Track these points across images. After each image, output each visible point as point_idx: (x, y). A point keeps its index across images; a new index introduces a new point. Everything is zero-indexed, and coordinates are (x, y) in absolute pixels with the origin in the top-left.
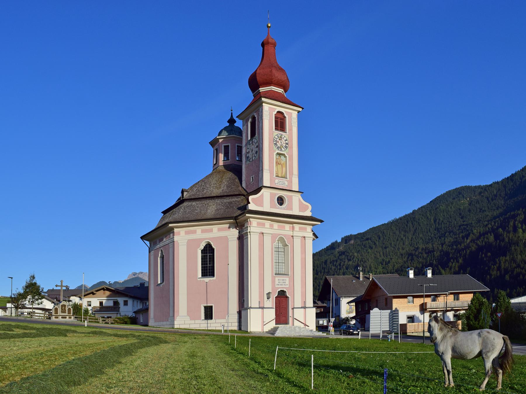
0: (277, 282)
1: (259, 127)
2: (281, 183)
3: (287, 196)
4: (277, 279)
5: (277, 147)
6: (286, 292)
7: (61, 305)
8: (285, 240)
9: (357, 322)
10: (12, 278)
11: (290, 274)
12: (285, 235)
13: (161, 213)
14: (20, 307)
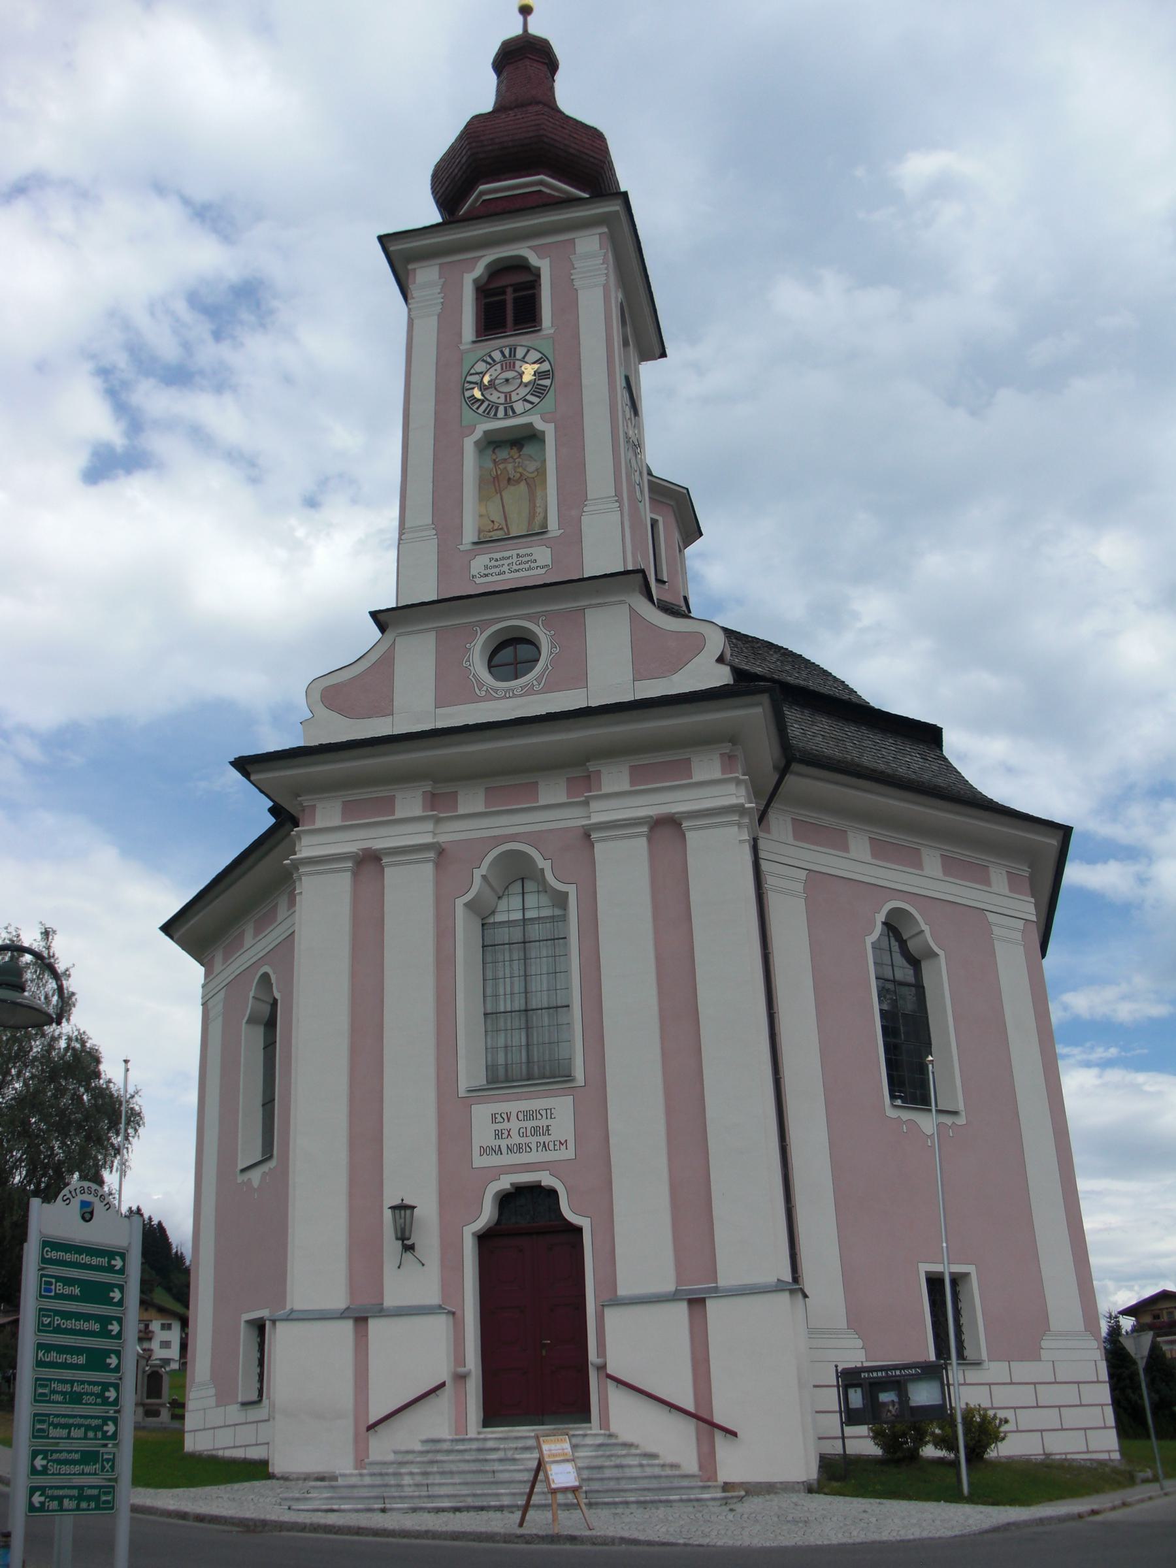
0: (482, 1132)
2: (505, 568)
3: (469, 694)
4: (481, 1113)
5: (535, 400)
6: (552, 1193)
8: (541, 863)
9: (701, 1423)
10: (268, 1444)
12: (534, 839)
13: (232, 763)
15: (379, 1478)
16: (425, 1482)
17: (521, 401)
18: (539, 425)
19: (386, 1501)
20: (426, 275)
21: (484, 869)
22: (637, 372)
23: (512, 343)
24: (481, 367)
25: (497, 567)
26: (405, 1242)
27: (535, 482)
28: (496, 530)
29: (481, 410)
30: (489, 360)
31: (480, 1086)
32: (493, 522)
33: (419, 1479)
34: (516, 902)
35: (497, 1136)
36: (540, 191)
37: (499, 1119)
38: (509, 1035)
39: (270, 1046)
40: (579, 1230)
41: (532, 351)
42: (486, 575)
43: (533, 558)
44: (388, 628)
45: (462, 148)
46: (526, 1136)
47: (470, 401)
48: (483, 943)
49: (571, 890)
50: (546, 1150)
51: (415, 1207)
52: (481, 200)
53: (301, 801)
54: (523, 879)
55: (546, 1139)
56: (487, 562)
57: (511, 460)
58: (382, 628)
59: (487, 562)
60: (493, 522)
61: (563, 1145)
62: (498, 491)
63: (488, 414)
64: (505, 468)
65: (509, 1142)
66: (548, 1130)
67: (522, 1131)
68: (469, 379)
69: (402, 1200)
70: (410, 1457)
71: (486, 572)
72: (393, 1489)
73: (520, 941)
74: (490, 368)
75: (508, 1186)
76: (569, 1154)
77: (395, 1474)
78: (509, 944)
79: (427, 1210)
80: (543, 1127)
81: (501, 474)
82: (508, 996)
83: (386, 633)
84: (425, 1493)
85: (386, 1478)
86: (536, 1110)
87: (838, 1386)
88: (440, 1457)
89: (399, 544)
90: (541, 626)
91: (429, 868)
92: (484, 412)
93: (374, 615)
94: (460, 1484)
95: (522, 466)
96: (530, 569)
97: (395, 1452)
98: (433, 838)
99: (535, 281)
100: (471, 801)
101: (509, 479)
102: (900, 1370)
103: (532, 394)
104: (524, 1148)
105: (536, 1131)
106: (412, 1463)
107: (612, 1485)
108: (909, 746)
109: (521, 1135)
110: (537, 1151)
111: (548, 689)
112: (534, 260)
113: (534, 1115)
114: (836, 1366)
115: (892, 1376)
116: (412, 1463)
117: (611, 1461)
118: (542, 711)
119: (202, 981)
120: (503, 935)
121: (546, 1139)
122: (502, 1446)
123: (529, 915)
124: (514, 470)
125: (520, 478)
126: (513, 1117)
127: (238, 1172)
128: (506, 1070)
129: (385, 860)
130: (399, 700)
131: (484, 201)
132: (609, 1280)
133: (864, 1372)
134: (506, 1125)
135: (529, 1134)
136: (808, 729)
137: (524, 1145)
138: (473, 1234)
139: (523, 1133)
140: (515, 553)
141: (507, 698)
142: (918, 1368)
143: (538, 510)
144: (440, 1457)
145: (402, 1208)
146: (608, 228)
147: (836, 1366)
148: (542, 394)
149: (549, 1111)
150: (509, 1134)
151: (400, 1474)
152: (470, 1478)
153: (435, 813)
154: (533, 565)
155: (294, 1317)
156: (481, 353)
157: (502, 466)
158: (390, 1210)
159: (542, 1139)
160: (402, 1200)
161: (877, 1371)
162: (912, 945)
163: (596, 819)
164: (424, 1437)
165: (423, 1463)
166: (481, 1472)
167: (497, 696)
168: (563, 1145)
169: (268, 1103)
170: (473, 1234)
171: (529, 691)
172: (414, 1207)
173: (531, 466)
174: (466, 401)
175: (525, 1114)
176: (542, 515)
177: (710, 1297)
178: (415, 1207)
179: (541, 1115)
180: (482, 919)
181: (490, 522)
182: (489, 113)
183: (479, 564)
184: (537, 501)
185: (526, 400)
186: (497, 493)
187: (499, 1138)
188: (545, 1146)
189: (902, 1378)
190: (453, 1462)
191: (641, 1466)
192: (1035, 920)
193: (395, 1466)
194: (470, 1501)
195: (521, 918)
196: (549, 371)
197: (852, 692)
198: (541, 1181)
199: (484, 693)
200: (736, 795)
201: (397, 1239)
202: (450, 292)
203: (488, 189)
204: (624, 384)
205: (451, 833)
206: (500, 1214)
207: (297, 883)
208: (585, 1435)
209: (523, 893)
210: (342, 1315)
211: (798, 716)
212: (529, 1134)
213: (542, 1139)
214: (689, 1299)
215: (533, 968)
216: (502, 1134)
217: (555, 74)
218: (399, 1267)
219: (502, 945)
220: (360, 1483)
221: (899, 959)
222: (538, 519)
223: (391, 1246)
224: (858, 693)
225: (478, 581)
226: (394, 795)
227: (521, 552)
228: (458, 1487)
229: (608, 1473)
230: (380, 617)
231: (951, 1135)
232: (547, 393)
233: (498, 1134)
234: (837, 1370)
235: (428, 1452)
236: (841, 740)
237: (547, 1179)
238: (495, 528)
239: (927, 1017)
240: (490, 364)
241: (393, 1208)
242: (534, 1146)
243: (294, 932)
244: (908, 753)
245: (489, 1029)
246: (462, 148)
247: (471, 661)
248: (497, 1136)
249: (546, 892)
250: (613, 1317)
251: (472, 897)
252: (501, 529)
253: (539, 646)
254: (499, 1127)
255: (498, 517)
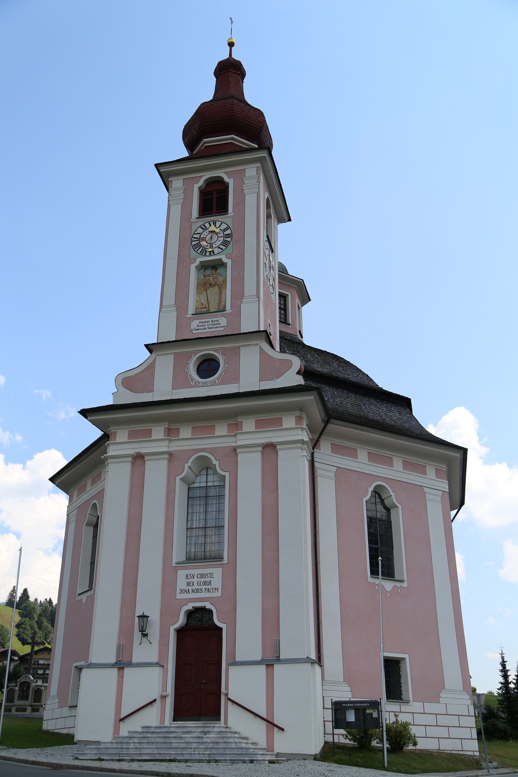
0: (181, 583)
1: (274, 235)
2: (206, 327)
3: (187, 384)
4: (181, 574)
5: (223, 248)
6: (210, 611)
7: (20, 683)
8: (215, 462)
11: (405, 578)
12: (212, 451)
14: (414, 738)
15: (120, 744)
16: (139, 747)
17: (217, 248)
18: (225, 260)
19: (121, 756)
20: (177, 183)
21: (189, 464)
22: (276, 229)
23: (214, 220)
24: (200, 230)
25: (202, 326)
26: (143, 633)
27: (222, 286)
28: (204, 308)
29: (199, 252)
30: (204, 227)
31: (183, 561)
32: (202, 304)
33: (137, 745)
34: (204, 478)
35: (188, 585)
36: (232, 142)
37: (189, 577)
38: (197, 539)
39: (95, 536)
40: (221, 629)
41: (223, 224)
42: (198, 330)
43: (219, 322)
44: (153, 351)
45: (196, 120)
46: (201, 585)
47: (194, 247)
48: (188, 496)
49: (227, 475)
50: (209, 592)
51: (149, 617)
52: (204, 146)
53: (110, 429)
54: (207, 468)
55: (209, 587)
56: (198, 323)
57: (212, 275)
58: (151, 352)
59: (198, 323)
60: (202, 304)
61: (216, 590)
62: (205, 290)
63: (202, 253)
64: (209, 279)
65: (193, 587)
66: (210, 583)
67: (199, 583)
68: (194, 236)
69: (143, 613)
70: (135, 735)
71: (198, 328)
72: (125, 750)
73: (204, 496)
74: (204, 231)
75: (191, 608)
76: (218, 594)
77: (127, 743)
78: (199, 497)
79: (155, 617)
80: (208, 581)
81: (207, 281)
82: (198, 521)
83: (152, 354)
84: (138, 752)
85: (123, 744)
86: (206, 574)
87: (332, 709)
88: (149, 735)
89: (160, 313)
90: (220, 354)
91: (165, 463)
92: (200, 252)
93: (147, 346)
94: (155, 748)
95: (216, 278)
96: (217, 327)
97: (129, 732)
98: (168, 449)
99: (227, 189)
100: (186, 432)
101: (211, 284)
102: (360, 703)
103: (222, 245)
104: (199, 591)
105: (205, 583)
106: (135, 737)
107: (222, 751)
108: (393, 408)
109: (198, 585)
110: (205, 592)
111: (222, 383)
112: (226, 179)
113: (205, 576)
114: (332, 700)
115: (356, 706)
116: (135, 737)
117: (223, 740)
118: (219, 393)
119: (68, 504)
120: (197, 493)
121: (209, 587)
122: (177, 731)
123: (209, 484)
124: (213, 280)
125: (216, 283)
126: (195, 577)
127: (77, 595)
128: (195, 554)
129: (146, 458)
130: (156, 385)
131: (206, 146)
132: (232, 653)
133: (344, 703)
134: (192, 580)
135: (202, 584)
136: (344, 400)
137: (199, 589)
138: (174, 629)
139: (199, 584)
140: (210, 320)
141: (204, 386)
142: (368, 703)
143: (223, 300)
144: (149, 735)
145: (143, 617)
146: (261, 164)
147: (332, 700)
148: (227, 245)
149: (211, 574)
150: (193, 584)
151: (129, 743)
152: (160, 746)
153: (169, 437)
154: (218, 326)
155: (91, 666)
156: (200, 224)
157: (208, 278)
158: (138, 617)
159: (207, 587)
160: (143, 613)
161: (349, 703)
162: (386, 501)
163: (239, 443)
164: (143, 725)
165: (140, 737)
166: (166, 743)
167: (199, 385)
168: (216, 590)
169: (93, 564)
170: (174, 629)
171: (214, 384)
172: (148, 617)
173: (221, 279)
174: (192, 246)
175: (201, 575)
176: (224, 302)
177: (275, 664)
178: (149, 617)
179: (208, 576)
180: (188, 485)
181: (201, 304)
182: (211, 101)
183: (194, 324)
184: (222, 296)
185: (219, 248)
186: (205, 291)
187: (188, 586)
188: (208, 590)
189: (361, 707)
190: (153, 737)
191: (236, 742)
192: (448, 491)
193: (128, 739)
194: (158, 757)
195: (206, 486)
196: (230, 234)
197: (371, 380)
198: (206, 606)
199: (194, 384)
200: (305, 436)
201: (140, 631)
202: (187, 192)
203: (208, 141)
204: (266, 239)
205: (175, 446)
206: (188, 620)
207: (107, 466)
208: (214, 727)
209: (207, 475)
210: (112, 666)
211: (340, 394)
212: (202, 584)
213: (207, 587)
214: (267, 664)
215: (209, 508)
216: (190, 584)
217: (244, 78)
218: (140, 644)
219: (196, 497)
220: (110, 747)
221: (380, 507)
222: (223, 304)
223: (137, 634)
224: (374, 381)
225: (194, 332)
226: (152, 429)
227: (214, 319)
228: (154, 750)
229: (221, 746)
230: (150, 347)
231: (400, 592)
232: (229, 245)
233: (188, 584)
234: (332, 702)
235: (143, 732)
236: (359, 406)
237: (208, 605)
238: (203, 307)
239: (392, 536)
240: (204, 229)
241: (138, 617)
242: (204, 590)
243: (104, 488)
244: (392, 411)
245: (189, 535)
246: (196, 120)
247: (189, 369)
248: (188, 585)
249: (217, 474)
250: (232, 669)
251: (185, 474)
252: (206, 308)
253: (219, 362)
254: (189, 581)
255: (204, 302)
